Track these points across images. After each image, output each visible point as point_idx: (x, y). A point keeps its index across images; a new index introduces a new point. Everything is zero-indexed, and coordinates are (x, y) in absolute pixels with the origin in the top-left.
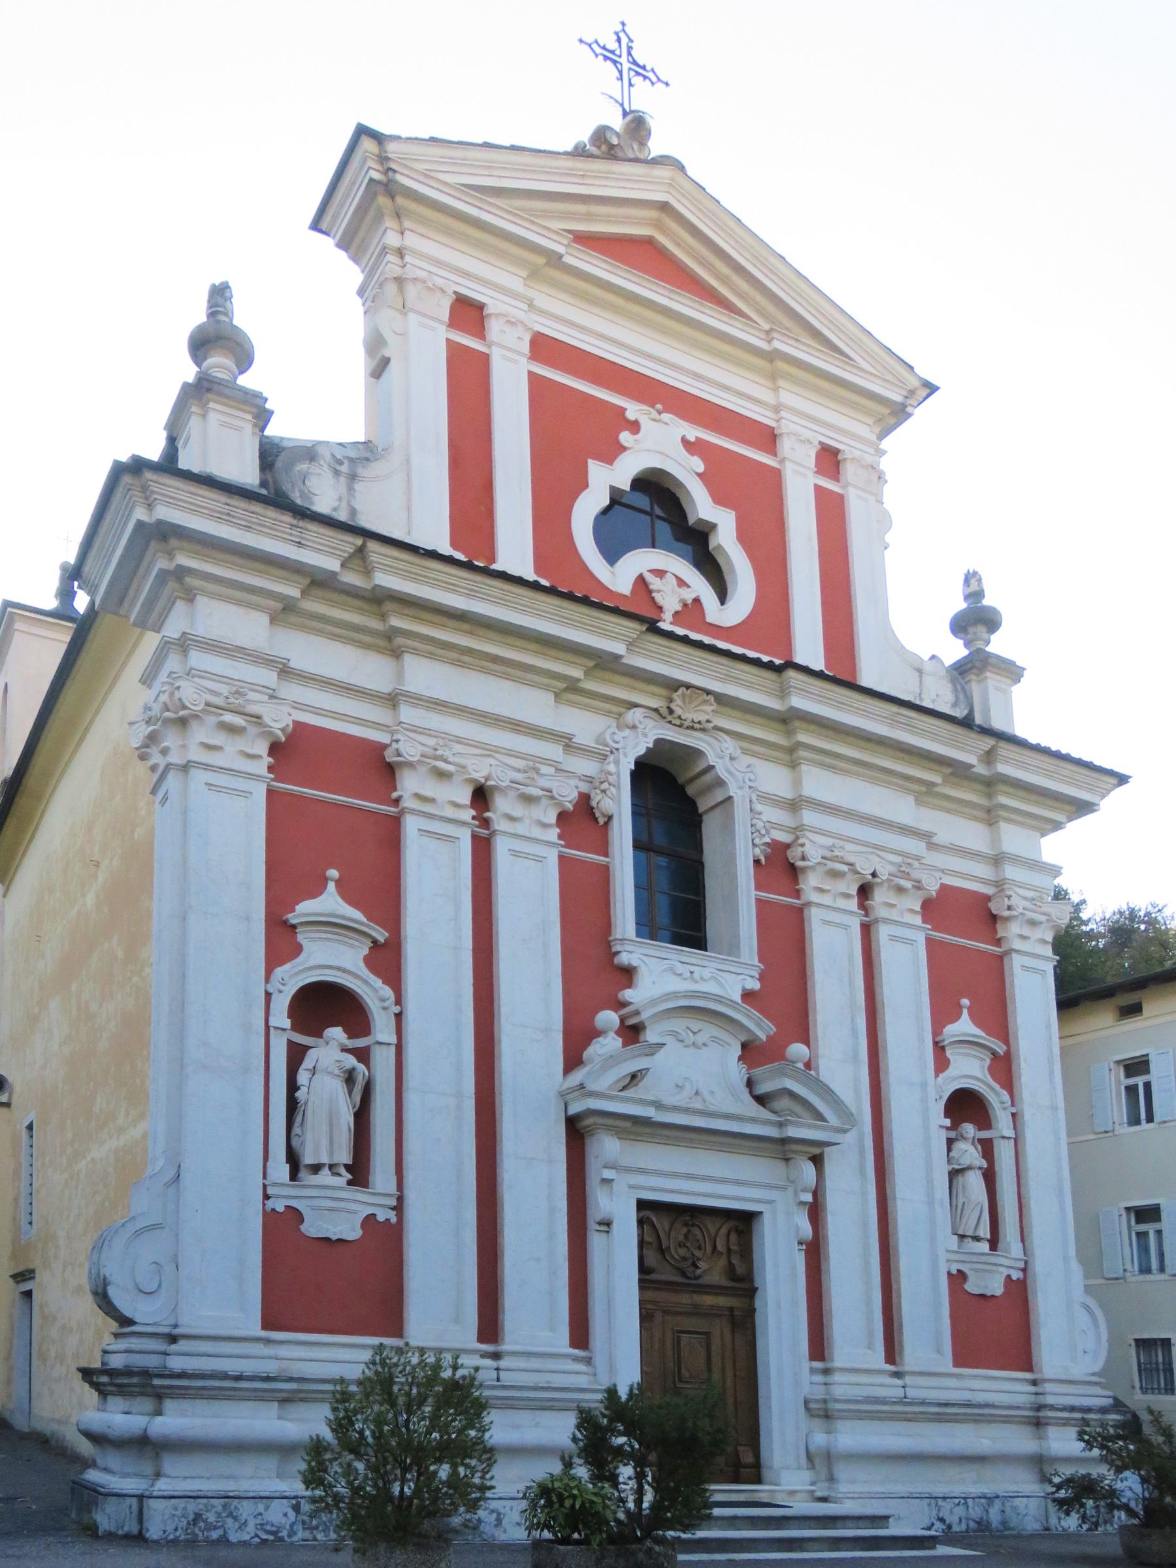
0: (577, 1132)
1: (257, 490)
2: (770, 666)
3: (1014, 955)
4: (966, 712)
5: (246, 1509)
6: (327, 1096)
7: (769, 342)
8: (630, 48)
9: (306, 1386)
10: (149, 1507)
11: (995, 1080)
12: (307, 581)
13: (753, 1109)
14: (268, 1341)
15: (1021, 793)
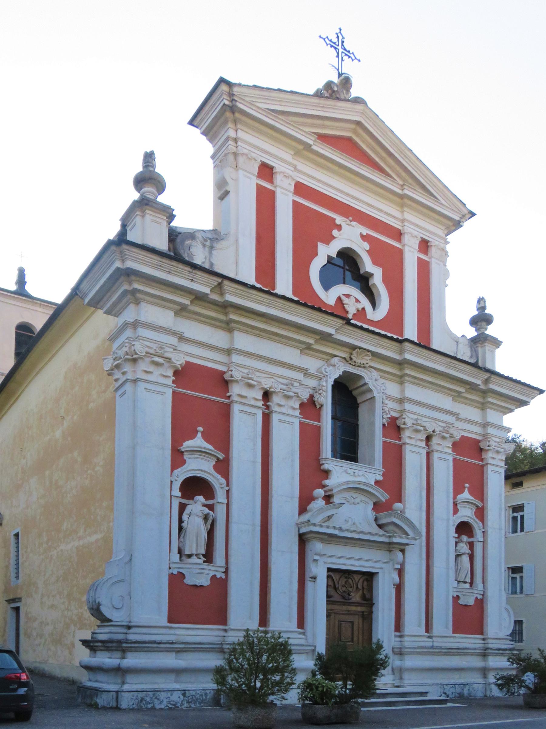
0: (303, 540)
1: (168, 253)
2: (397, 340)
3: (489, 466)
4: (475, 361)
5: (163, 696)
6: (196, 526)
7: (402, 190)
8: (343, 42)
9: (187, 646)
10: (122, 696)
11: (477, 518)
12: (193, 297)
13: (376, 530)
14: (454, 637)
15: (498, 397)
